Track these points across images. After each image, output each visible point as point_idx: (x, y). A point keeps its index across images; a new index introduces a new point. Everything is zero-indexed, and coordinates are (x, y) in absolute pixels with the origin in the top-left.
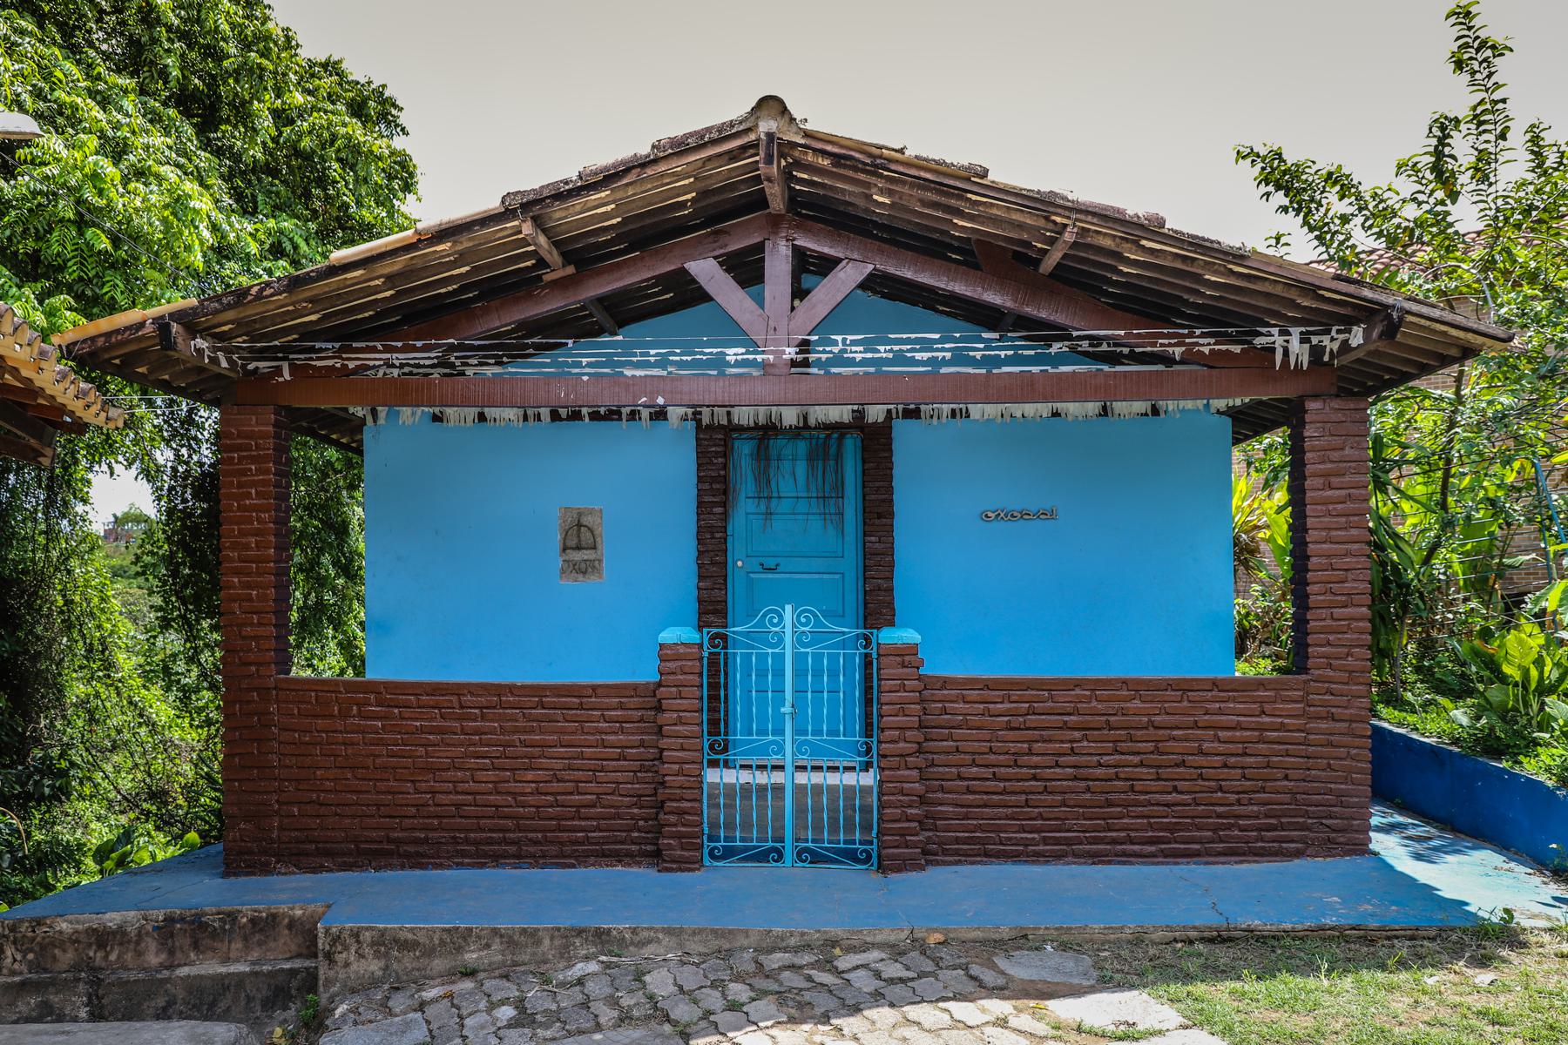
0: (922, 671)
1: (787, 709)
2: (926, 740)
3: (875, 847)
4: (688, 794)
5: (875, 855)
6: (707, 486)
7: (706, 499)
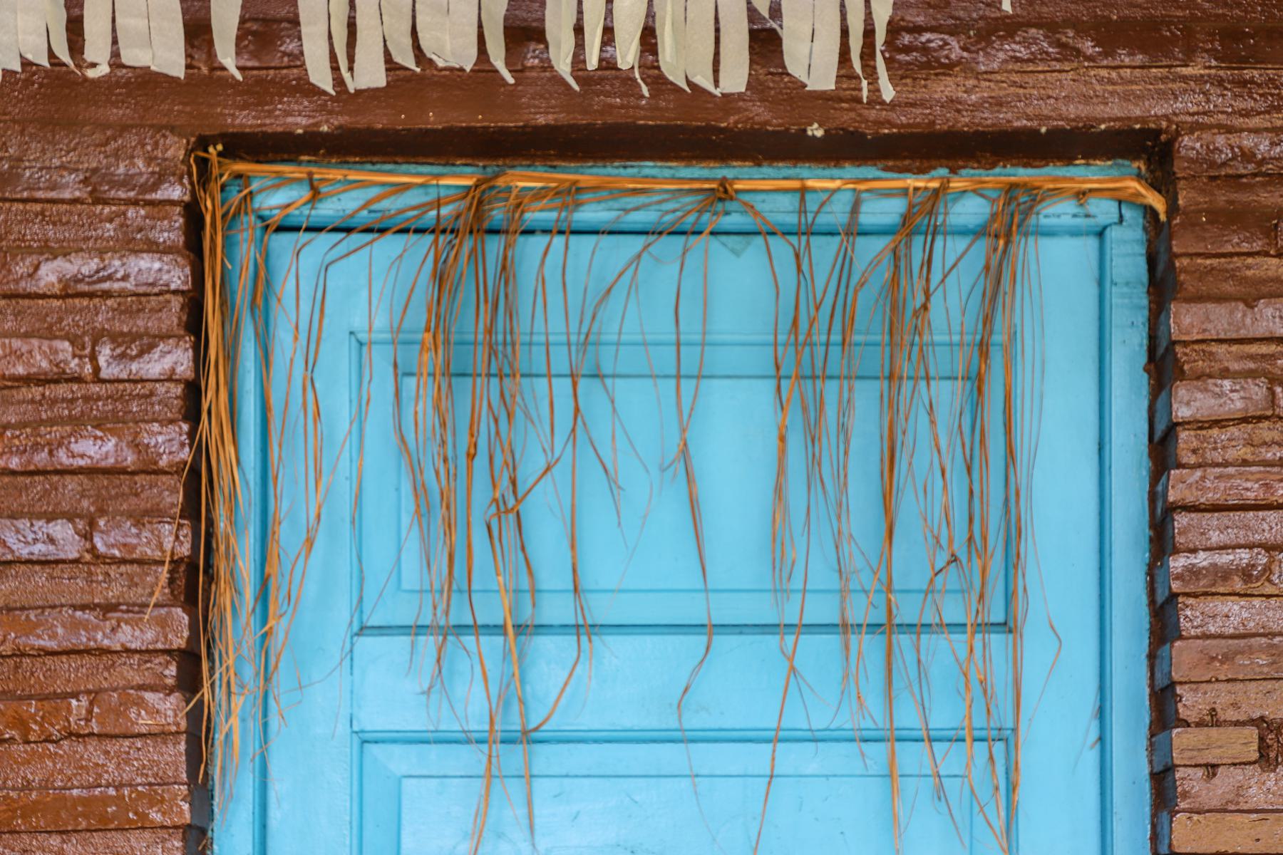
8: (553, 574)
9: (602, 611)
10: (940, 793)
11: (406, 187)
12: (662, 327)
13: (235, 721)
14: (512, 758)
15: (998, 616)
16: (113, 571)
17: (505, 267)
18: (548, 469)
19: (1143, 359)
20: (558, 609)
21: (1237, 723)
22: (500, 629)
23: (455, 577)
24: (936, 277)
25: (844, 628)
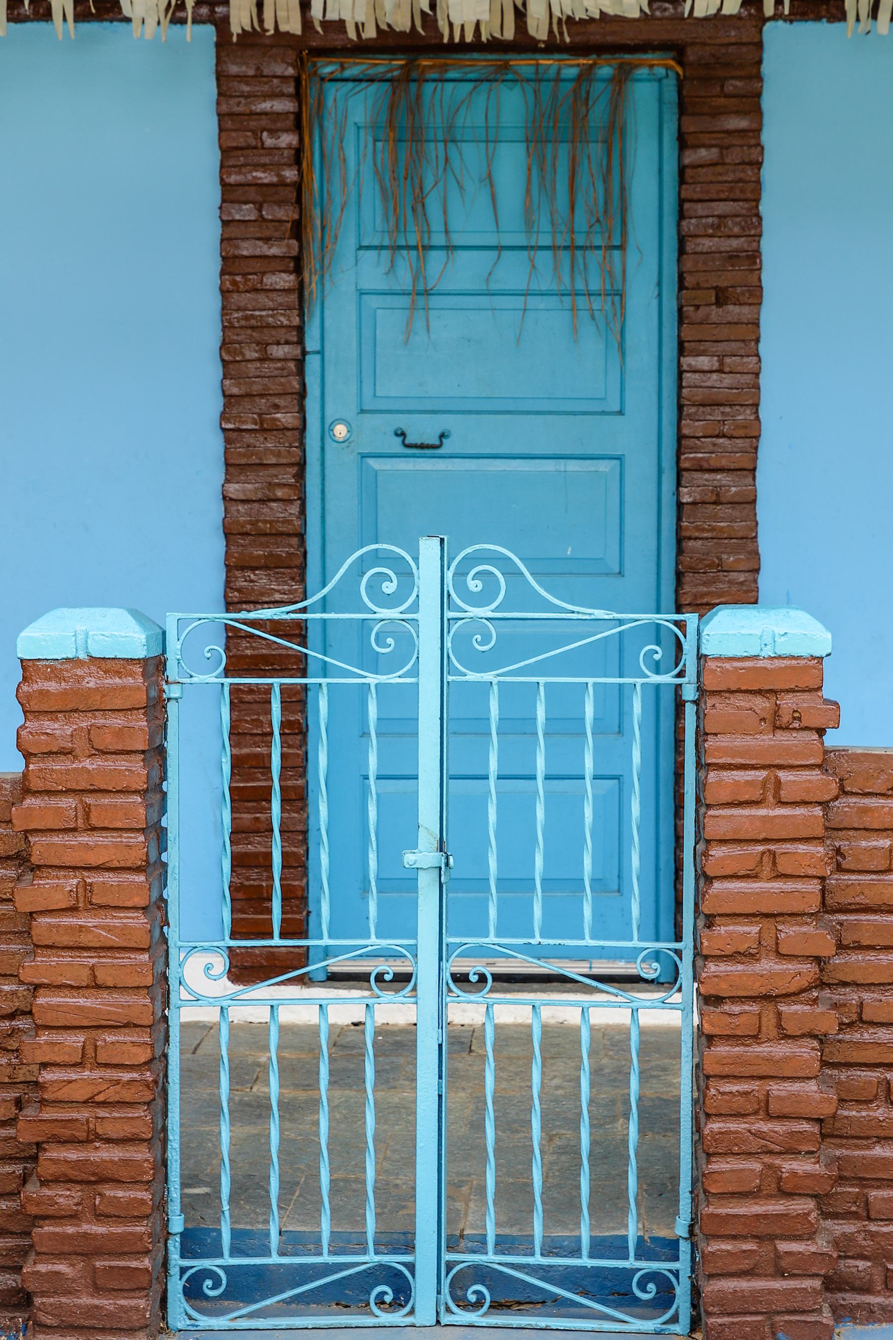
0: (832, 739)
1: (423, 856)
2: (841, 947)
3: (683, 1265)
4: (113, 1122)
5: (682, 1291)
6: (247, 212)
7: (247, 249)
8: (436, 224)
9: (457, 240)
10: (593, 317)
11: (376, 65)
12: (481, 122)
13: (313, 285)
14: (421, 301)
15: (617, 242)
16: (269, 224)
17: (419, 97)
18: (436, 184)
19: (676, 135)
20: (438, 239)
21: (708, 288)
22: (416, 248)
23: (398, 228)
24: (590, 103)
25: (554, 248)
